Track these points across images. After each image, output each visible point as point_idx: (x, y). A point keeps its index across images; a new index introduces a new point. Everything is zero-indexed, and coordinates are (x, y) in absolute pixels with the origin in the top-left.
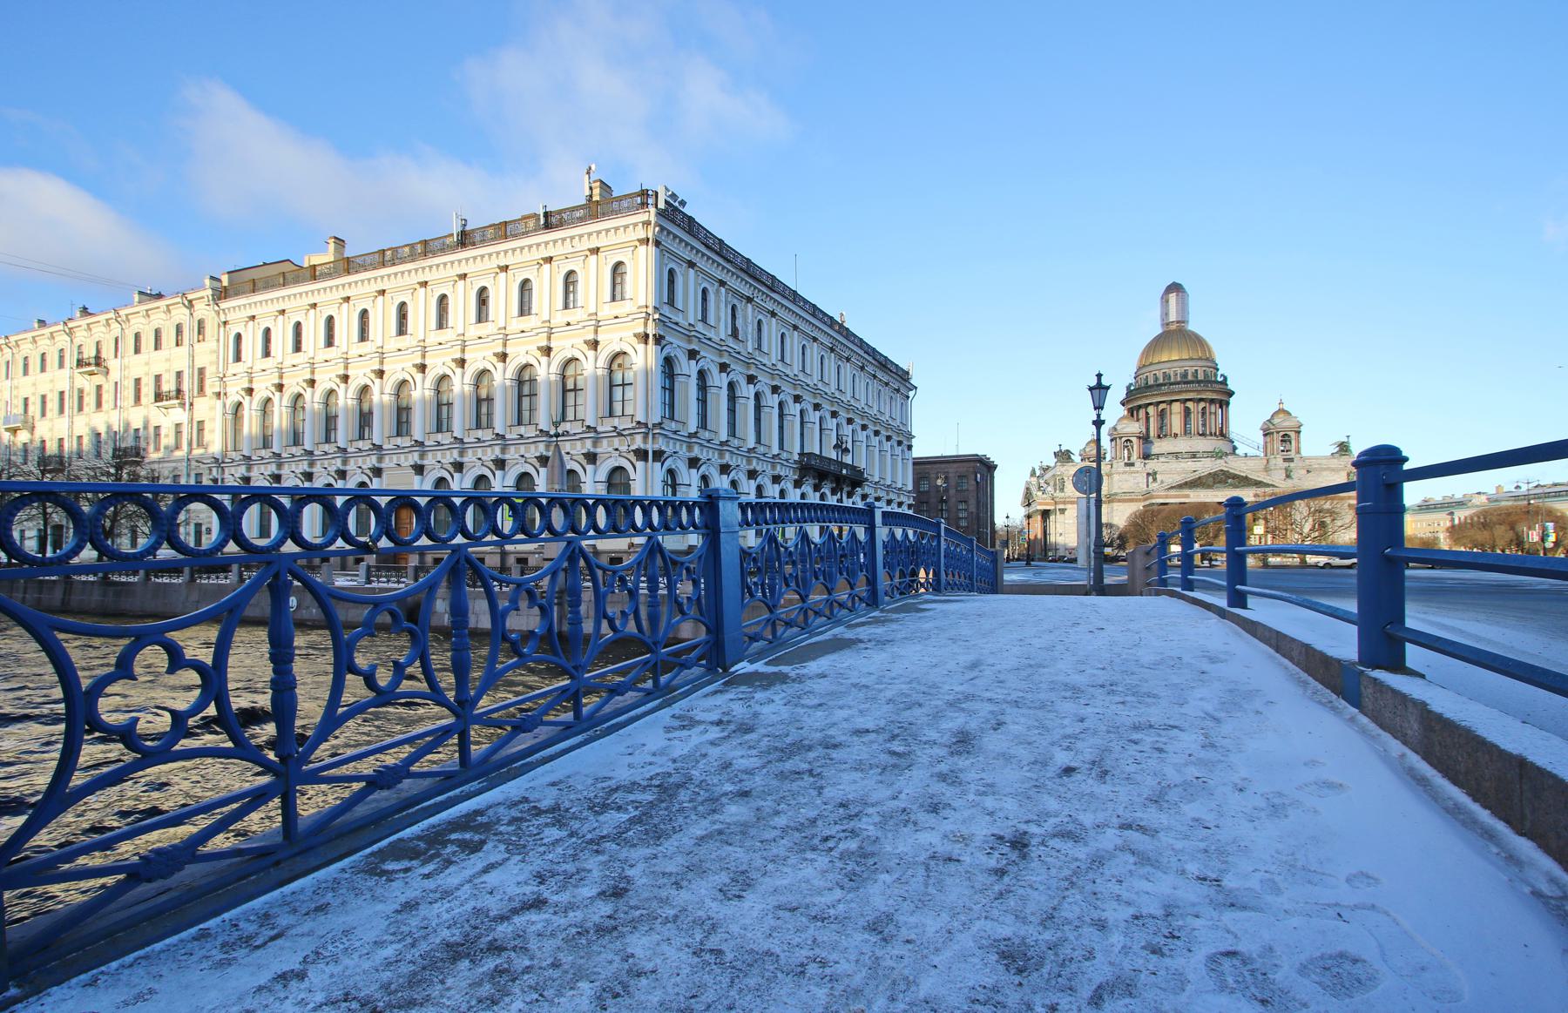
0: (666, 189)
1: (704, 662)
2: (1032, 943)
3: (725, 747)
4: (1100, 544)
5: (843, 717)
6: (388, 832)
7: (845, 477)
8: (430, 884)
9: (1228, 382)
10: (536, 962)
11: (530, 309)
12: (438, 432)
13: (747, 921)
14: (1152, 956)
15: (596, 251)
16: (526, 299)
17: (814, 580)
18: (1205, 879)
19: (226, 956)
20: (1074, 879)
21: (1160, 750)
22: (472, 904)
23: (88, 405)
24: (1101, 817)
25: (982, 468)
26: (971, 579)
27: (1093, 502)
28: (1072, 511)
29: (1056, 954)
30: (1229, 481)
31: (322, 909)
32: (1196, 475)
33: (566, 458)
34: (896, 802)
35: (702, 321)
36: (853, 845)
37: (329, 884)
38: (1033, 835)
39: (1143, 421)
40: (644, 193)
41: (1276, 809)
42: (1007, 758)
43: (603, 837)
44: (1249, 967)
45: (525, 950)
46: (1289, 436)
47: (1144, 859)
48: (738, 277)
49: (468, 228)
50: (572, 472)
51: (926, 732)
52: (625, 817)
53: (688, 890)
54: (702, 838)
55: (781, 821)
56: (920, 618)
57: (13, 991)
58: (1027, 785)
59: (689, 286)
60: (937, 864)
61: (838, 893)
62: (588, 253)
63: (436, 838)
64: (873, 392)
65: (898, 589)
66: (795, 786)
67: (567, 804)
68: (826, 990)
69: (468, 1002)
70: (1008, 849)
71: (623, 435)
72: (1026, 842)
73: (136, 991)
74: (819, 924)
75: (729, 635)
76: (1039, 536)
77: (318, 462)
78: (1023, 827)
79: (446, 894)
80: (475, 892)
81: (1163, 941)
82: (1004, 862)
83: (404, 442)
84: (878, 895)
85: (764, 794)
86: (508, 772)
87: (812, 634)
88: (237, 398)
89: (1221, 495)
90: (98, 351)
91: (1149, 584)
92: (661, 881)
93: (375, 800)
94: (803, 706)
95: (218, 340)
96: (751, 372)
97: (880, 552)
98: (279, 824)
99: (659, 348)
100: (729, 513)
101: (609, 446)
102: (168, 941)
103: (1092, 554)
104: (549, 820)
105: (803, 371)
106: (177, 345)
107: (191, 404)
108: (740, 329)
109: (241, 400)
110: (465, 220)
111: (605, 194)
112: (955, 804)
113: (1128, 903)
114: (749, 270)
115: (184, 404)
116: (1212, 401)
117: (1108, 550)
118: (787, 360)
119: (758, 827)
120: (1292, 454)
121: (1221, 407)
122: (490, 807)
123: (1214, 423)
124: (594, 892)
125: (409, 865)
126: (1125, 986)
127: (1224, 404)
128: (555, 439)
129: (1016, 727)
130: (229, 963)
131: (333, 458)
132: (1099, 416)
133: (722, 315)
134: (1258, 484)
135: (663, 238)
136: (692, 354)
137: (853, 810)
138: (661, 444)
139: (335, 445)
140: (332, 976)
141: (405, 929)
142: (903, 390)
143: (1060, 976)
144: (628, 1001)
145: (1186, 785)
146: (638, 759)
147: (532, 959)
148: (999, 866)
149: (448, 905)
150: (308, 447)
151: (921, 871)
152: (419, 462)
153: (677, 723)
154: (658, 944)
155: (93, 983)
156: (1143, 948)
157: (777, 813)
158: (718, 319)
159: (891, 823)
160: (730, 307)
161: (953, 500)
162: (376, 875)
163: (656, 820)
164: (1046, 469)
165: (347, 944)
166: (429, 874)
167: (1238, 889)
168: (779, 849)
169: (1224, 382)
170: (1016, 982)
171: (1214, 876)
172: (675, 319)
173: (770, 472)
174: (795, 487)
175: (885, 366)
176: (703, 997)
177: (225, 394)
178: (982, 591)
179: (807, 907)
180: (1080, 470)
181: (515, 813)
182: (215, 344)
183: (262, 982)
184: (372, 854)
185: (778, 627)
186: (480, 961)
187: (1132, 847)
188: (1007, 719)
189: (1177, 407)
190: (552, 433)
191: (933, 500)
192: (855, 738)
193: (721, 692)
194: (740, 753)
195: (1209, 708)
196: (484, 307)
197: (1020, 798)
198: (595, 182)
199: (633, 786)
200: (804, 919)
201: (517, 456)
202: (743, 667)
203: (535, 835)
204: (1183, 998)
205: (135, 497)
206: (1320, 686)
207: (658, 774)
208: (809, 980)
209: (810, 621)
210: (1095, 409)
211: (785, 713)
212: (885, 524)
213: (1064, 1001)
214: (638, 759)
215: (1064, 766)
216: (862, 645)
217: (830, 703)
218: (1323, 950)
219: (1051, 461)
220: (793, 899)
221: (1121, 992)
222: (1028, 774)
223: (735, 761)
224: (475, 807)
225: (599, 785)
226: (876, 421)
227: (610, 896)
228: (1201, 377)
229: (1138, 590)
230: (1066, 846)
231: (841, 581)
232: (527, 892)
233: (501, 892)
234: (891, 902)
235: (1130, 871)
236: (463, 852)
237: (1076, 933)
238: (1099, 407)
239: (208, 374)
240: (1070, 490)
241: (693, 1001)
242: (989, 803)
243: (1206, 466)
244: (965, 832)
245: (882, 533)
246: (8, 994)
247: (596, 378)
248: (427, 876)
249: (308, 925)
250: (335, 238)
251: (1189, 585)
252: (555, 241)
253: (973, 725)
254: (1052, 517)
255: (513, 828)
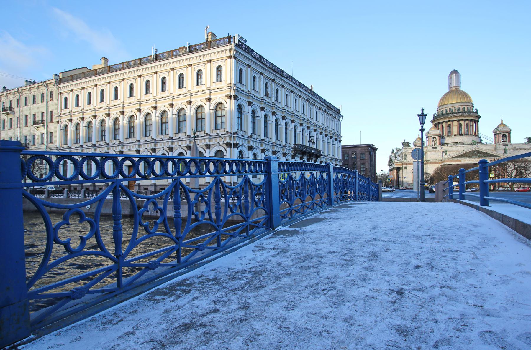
0: (239, 35)
1: (265, 226)
2: (409, 327)
3: (278, 258)
4: (423, 182)
5: (324, 247)
6: (154, 286)
7: (313, 154)
8: (173, 304)
9: (478, 112)
10: (219, 330)
11: (183, 85)
12: (146, 136)
13: (297, 318)
14: (457, 332)
15: (210, 61)
16: (181, 82)
17: (307, 194)
18: (476, 306)
19: (104, 327)
20: (423, 305)
21: (455, 259)
22: (190, 311)
23: (6, 126)
24: (432, 283)
25: (371, 150)
26: (368, 195)
27: (420, 163)
28: (410, 168)
29: (419, 330)
30: (479, 154)
31: (135, 312)
32: (464, 152)
33: (198, 146)
34: (349, 278)
35: (253, 89)
36: (334, 292)
37: (136, 304)
38: (405, 290)
39: (440, 129)
40: (229, 37)
41: (505, 282)
42: (392, 262)
43: (236, 289)
44: (497, 336)
45: (214, 326)
46: (506, 135)
47: (451, 298)
48: (268, 71)
49: (157, 53)
50: (200, 152)
51: (358, 252)
52: (243, 282)
53: (272, 307)
54: (274, 289)
55: (304, 284)
56: (350, 210)
57: (32, 336)
58: (401, 272)
59: (248, 74)
60: (368, 299)
61: (330, 309)
62: (207, 62)
63: (172, 289)
64: (325, 118)
65: (339, 199)
66: (308, 271)
67: (220, 277)
68: (331, 341)
69: (197, 343)
70: (396, 294)
71: (221, 137)
72: (403, 292)
73: (75, 337)
74: (325, 319)
75: (275, 215)
76: (396, 178)
77: (98, 149)
78: (401, 287)
79: (180, 307)
80: (191, 307)
81: (461, 327)
82: (395, 299)
83: (132, 140)
84: (346, 310)
85: (297, 274)
86: (195, 265)
87: (306, 216)
88: (66, 123)
89: (476, 161)
90: (11, 104)
91: (444, 198)
92: (261, 304)
93: (147, 275)
94: (307, 242)
95: (58, 100)
96: (274, 111)
97: (333, 184)
98: (115, 282)
99: (236, 101)
100: (274, 166)
101: (177, 144)
102: (82, 321)
103: (420, 185)
104: (214, 283)
105: (295, 110)
106: (42, 102)
107: (47, 126)
108: (269, 93)
109: (67, 124)
110: (157, 50)
111: (213, 37)
112: (373, 278)
113: (446, 314)
114: (273, 68)
115: (45, 126)
116: (471, 120)
117: (426, 184)
118: (289, 105)
119: (296, 286)
120: (507, 143)
121: (475, 123)
122: (190, 278)
123: (472, 130)
124: (236, 307)
125: (164, 297)
126: (448, 342)
127: (476, 122)
128: (194, 139)
129: (395, 251)
130: (106, 329)
131: (104, 147)
132: (422, 127)
133: (262, 87)
134: (492, 156)
135: (237, 56)
136: (250, 103)
137: (332, 280)
138: (237, 141)
139: (105, 142)
140: (145, 333)
141: (168, 319)
142: (337, 117)
143: (421, 338)
144: (256, 343)
145: (466, 272)
146: (244, 261)
147: (218, 329)
148: (393, 300)
149: (182, 311)
150: (94, 143)
151: (362, 302)
152: (138, 149)
153: (257, 249)
154: (264, 325)
155: (59, 334)
156: (453, 329)
157: (302, 281)
158: (260, 89)
159: (348, 285)
160: (265, 84)
161: (359, 163)
162: (152, 300)
163: (255, 283)
164: (398, 150)
165: (148, 324)
166: (172, 300)
167: (490, 309)
168: (306, 293)
169: (477, 112)
170: (404, 339)
171: (480, 305)
172: (242, 89)
173: (282, 152)
174: (292, 158)
175: (330, 107)
176: (285, 342)
177: (61, 122)
178: (373, 200)
179: (319, 313)
180: (414, 150)
181: (200, 280)
182: (57, 101)
183: (120, 335)
184: (149, 293)
185: (305, 209)
186: (198, 329)
187: (446, 294)
188: (390, 248)
189: (455, 123)
190: (192, 136)
191: (350, 164)
192: (330, 255)
193: (273, 237)
194: (284, 260)
195: (475, 244)
196: (164, 85)
197: (398, 276)
198: (209, 33)
199: (244, 271)
200: (318, 317)
201: (178, 146)
202: (280, 228)
203: (209, 288)
204: (471, 346)
205: (70, 157)
206: (522, 236)
207: (253, 267)
208: (324, 337)
209: (293, 215)
210: (421, 124)
211: (300, 245)
212: (334, 172)
213: (423, 346)
214: (244, 261)
215: (416, 265)
216: (327, 220)
217: (318, 242)
218: (526, 331)
219: (401, 146)
220: (313, 311)
221: (445, 343)
222: (401, 268)
223: (282, 263)
224: (184, 278)
225: (231, 271)
226: (326, 130)
227: (243, 309)
228: (466, 110)
229: (440, 200)
230: (419, 293)
231: (308, 197)
232: (211, 307)
233: (201, 307)
234: (351, 312)
235: (446, 303)
236: (183, 293)
237: (425, 324)
238: (422, 123)
239: (54, 113)
240: (410, 158)
241: (280, 343)
242: (387, 278)
243: (468, 148)
244: (378, 288)
245: (333, 176)
246: (30, 337)
247: (210, 113)
248: (172, 301)
249: (131, 317)
250: (104, 58)
251: (462, 197)
252: (193, 58)
253: (377, 250)
254: (401, 171)
255: (201, 285)
